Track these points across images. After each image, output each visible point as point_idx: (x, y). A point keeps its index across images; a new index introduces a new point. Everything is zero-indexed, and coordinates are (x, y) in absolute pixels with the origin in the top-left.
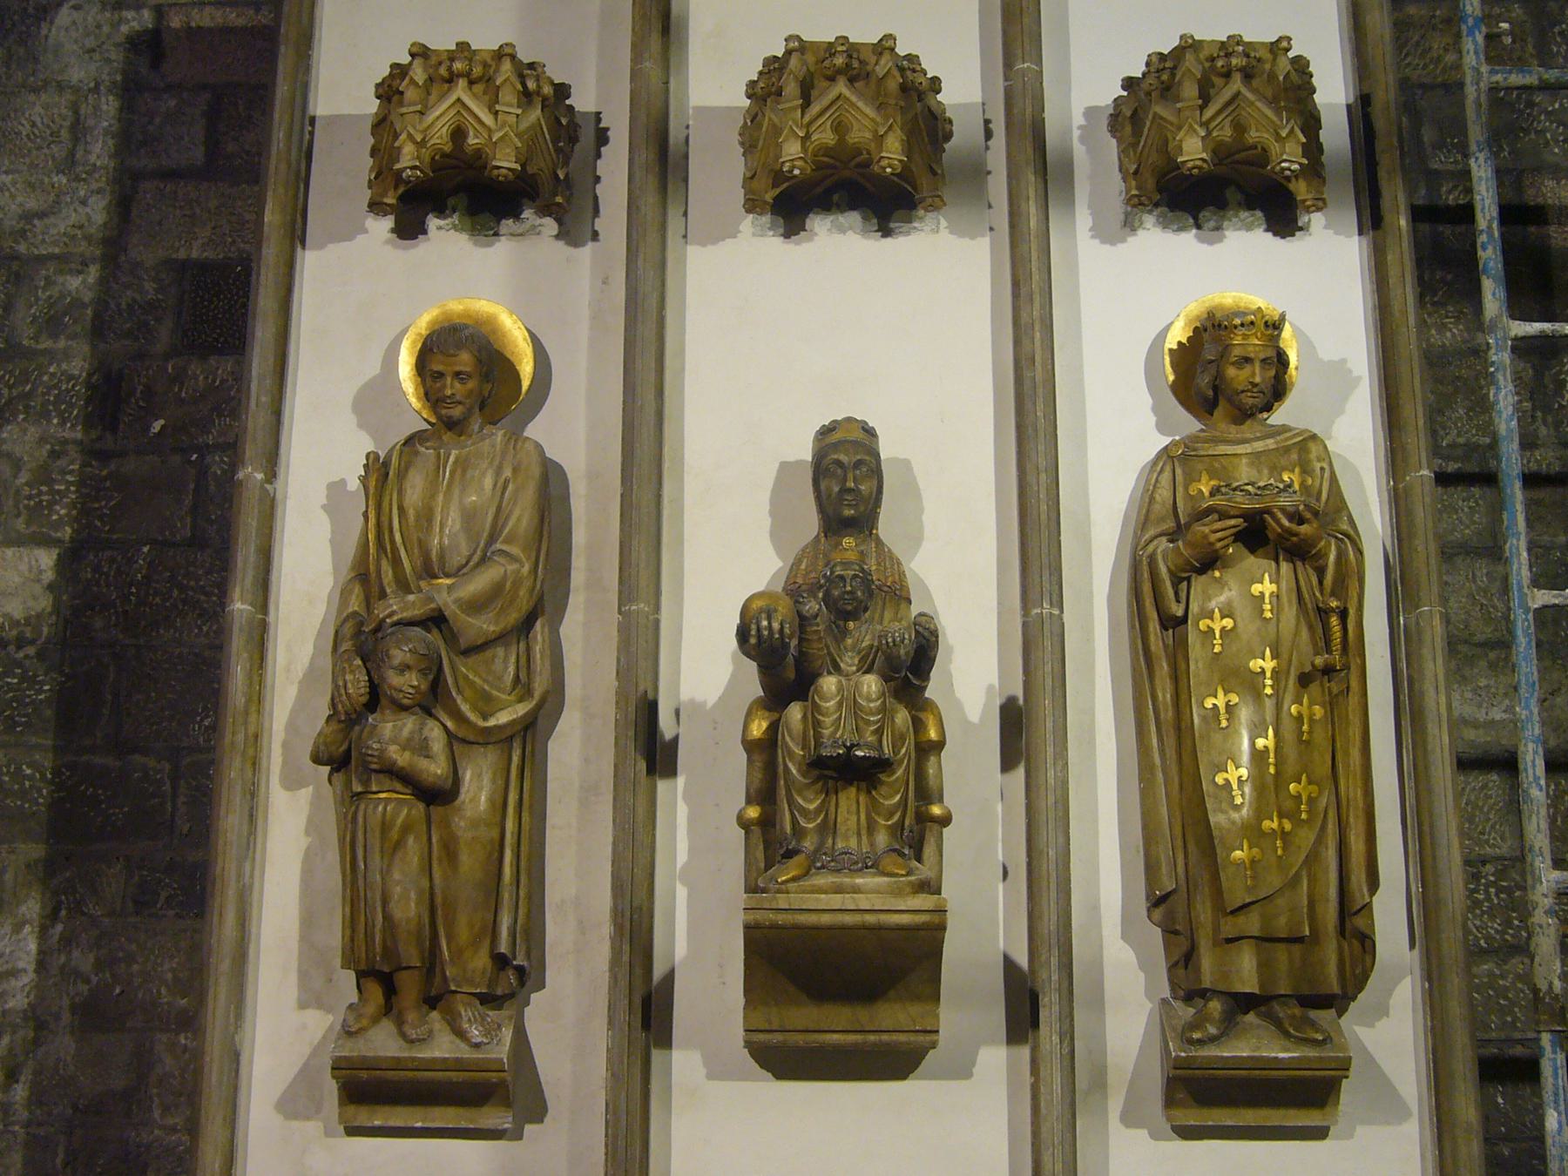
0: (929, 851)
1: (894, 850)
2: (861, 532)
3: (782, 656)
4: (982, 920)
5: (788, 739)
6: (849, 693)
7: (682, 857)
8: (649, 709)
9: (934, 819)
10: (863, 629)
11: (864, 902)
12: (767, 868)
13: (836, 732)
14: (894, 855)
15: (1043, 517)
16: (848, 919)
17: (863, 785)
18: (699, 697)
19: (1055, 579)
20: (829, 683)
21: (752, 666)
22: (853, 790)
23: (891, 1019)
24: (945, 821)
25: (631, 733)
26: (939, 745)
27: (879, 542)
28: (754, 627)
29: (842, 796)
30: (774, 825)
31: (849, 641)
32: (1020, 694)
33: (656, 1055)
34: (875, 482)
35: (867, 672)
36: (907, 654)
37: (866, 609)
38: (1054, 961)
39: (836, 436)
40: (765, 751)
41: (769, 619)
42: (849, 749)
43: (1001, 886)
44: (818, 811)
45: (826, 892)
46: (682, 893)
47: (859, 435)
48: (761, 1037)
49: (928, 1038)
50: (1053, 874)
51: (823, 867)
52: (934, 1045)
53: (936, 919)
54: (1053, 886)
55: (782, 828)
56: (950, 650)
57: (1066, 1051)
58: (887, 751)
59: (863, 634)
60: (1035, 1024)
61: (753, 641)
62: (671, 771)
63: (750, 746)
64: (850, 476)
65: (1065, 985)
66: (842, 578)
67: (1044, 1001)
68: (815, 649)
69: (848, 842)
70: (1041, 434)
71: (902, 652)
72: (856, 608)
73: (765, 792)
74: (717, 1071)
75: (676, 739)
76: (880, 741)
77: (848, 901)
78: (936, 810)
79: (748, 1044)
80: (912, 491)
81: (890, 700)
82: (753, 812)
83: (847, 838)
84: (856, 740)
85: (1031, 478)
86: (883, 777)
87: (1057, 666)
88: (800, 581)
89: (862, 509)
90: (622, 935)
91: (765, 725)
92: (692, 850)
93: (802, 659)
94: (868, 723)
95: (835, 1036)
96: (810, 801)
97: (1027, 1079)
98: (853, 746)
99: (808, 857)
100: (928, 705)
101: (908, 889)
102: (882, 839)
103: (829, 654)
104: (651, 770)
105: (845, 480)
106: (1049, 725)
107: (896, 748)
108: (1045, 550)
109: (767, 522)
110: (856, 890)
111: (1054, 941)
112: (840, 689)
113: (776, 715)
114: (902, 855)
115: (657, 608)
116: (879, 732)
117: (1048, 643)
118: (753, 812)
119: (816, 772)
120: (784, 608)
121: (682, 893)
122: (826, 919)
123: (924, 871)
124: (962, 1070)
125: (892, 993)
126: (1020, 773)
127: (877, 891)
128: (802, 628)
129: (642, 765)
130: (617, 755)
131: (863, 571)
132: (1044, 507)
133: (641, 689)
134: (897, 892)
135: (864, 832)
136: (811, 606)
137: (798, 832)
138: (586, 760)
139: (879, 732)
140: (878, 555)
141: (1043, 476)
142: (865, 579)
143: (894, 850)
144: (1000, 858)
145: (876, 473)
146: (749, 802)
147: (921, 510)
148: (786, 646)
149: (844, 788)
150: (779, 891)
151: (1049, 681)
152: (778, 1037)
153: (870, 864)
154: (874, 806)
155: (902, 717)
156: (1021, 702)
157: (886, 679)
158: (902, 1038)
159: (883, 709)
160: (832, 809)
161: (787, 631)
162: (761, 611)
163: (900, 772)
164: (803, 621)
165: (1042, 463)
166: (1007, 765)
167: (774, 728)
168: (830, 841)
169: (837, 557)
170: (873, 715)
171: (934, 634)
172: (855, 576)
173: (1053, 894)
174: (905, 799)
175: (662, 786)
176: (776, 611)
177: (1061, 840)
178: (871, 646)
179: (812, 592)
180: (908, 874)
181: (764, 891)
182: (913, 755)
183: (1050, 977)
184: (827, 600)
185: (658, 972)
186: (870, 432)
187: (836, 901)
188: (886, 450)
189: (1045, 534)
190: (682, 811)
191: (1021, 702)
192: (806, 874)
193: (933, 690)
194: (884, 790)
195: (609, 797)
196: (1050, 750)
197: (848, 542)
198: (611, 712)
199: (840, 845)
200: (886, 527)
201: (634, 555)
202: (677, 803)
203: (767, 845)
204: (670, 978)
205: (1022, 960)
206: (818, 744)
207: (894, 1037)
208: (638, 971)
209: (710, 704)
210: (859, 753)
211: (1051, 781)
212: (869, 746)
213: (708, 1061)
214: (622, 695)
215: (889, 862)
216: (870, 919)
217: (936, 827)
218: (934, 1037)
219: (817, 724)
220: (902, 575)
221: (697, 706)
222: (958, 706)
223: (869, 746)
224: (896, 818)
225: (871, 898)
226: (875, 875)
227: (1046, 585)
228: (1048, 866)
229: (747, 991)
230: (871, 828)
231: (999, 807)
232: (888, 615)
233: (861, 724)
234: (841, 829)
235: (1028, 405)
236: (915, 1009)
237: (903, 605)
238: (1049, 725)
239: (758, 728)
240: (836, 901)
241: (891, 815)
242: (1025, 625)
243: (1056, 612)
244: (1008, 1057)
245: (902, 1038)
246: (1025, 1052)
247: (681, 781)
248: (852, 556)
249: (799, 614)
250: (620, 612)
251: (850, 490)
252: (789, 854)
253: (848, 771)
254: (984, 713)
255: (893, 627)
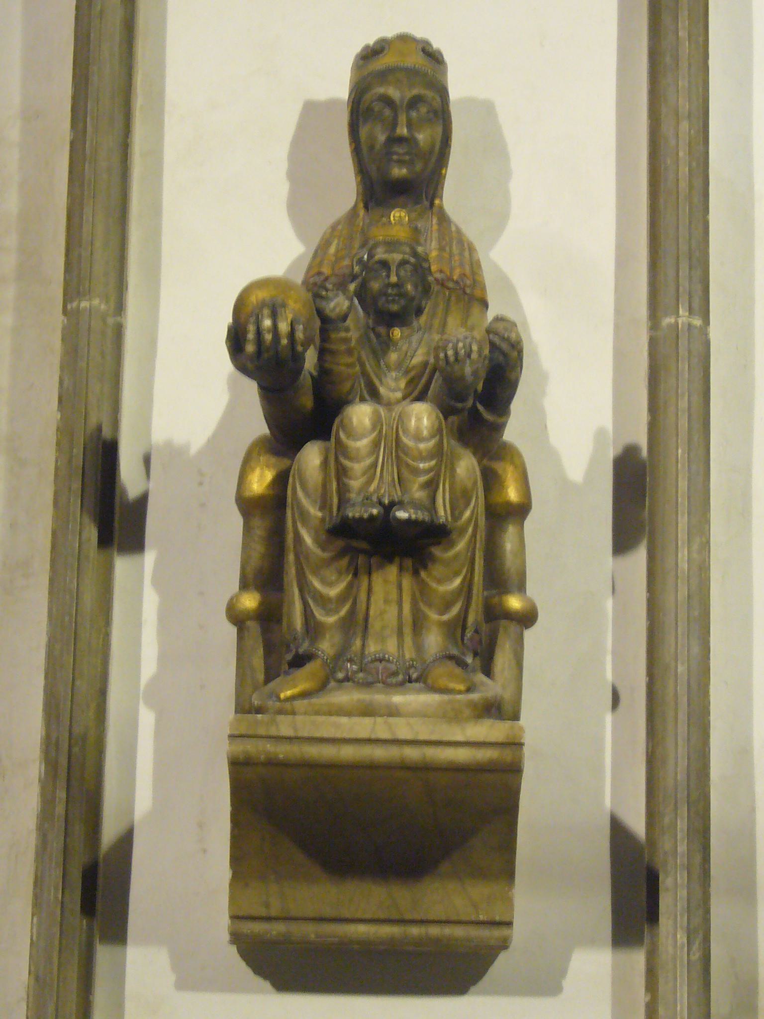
0: (502, 660)
1: (451, 658)
2: (417, 202)
3: (294, 374)
4: (577, 765)
5: (300, 494)
6: (389, 430)
7: (149, 667)
8: (106, 454)
9: (510, 616)
10: (415, 338)
11: (403, 729)
12: (268, 679)
13: (369, 486)
14: (451, 666)
15: (683, 185)
16: (380, 753)
17: (409, 563)
18: (179, 437)
19: (697, 273)
20: (361, 414)
21: (251, 388)
22: (392, 571)
23: (443, 903)
24: (528, 618)
25: (77, 485)
26: (522, 510)
27: (443, 219)
28: (252, 328)
29: (378, 579)
30: (279, 621)
31: (393, 357)
32: (643, 441)
33: (103, 954)
34: (439, 130)
35: (420, 398)
36: (475, 373)
37: (419, 311)
38: (682, 825)
39: (386, 60)
40: (268, 513)
41: (274, 316)
42: (388, 508)
43: (609, 718)
44: (342, 599)
45: (349, 714)
46: (147, 719)
47: (416, 60)
48: (257, 928)
49: (497, 933)
50: (683, 700)
51: (347, 679)
52: (504, 945)
53: (507, 755)
54: (682, 717)
55: (290, 625)
56: (543, 378)
57: (696, 956)
58: (443, 513)
59: (413, 347)
60: (653, 916)
61: (250, 348)
62: (135, 543)
63: (248, 506)
64: (402, 118)
65: (698, 859)
66: (385, 264)
67: (666, 882)
68: (343, 366)
69: (385, 644)
70: (684, 64)
71: (468, 370)
72: (405, 309)
73: (268, 573)
74: (189, 979)
75: (143, 500)
76: (433, 500)
77: (379, 728)
78: (514, 603)
79: (236, 938)
80: (495, 147)
81: (450, 443)
82: (250, 602)
83: (382, 639)
84: (397, 494)
85: (667, 128)
86: (436, 551)
87: (697, 400)
88: (326, 270)
89: (418, 167)
90: (55, 777)
91: (269, 476)
92: (163, 658)
93: (324, 376)
94: (416, 472)
95: (362, 930)
96: (331, 584)
97: (641, 996)
98: (392, 504)
99: (325, 663)
100: (507, 453)
101: (467, 712)
102: (434, 641)
103: (364, 374)
104: (106, 540)
105: (394, 124)
106: (683, 485)
107: (455, 510)
108: (683, 232)
109: (283, 188)
110: (393, 712)
111: (682, 795)
112: (377, 422)
113: (286, 462)
114: (461, 663)
115: (120, 307)
116: (431, 486)
117: (684, 366)
118: (250, 602)
119: (340, 543)
120: (296, 306)
121: (147, 719)
122: (348, 753)
123: (492, 688)
124: (546, 983)
125: (445, 867)
126: (639, 557)
127: (422, 714)
128: (324, 333)
129: (92, 533)
130: (56, 518)
131: (415, 254)
132: (684, 170)
133: (93, 421)
134: (454, 716)
135: (408, 630)
136: (338, 304)
137: (313, 629)
138: (13, 526)
139: (431, 486)
140: (441, 239)
141: (684, 126)
142: (419, 267)
143: (451, 658)
144: (609, 675)
145: (441, 115)
146: (244, 585)
147: (506, 174)
148: (297, 358)
149: (381, 567)
150: (281, 712)
151: (683, 423)
152: (277, 929)
153: (415, 676)
154: (422, 592)
155: (466, 465)
156: (644, 453)
157: (447, 411)
158: (458, 932)
159: (438, 453)
160: (363, 596)
161: (300, 335)
162: (263, 304)
163: (461, 545)
164: (327, 324)
165: (684, 106)
166: (622, 544)
167: (282, 480)
168: (358, 643)
169: (379, 234)
170: (423, 459)
171: (517, 347)
172: (403, 263)
173: (682, 729)
174: (468, 585)
175: (122, 565)
176: (284, 305)
177: (696, 650)
178: (425, 364)
179: (342, 286)
180: (469, 690)
181: (259, 710)
182: (482, 522)
183: (675, 849)
184: (362, 294)
185: (109, 832)
186: (435, 58)
187: (363, 727)
188: (459, 86)
189: (684, 209)
190: (151, 601)
191: (644, 453)
192: (322, 687)
193: (514, 432)
194: (437, 570)
195: (44, 579)
196: (683, 522)
197: (397, 214)
198: (49, 456)
199: (373, 648)
200: (455, 195)
201: (87, 228)
202: (142, 587)
203: (269, 649)
204: (126, 841)
205: (637, 824)
206: (343, 501)
207: (448, 931)
208: (78, 829)
209: (194, 450)
210: (402, 515)
211: (683, 565)
212: (416, 505)
213: (178, 963)
214: (65, 431)
215: (443, 674)
216: (412, 754)
217: (513, 627)
218: (504, 931)
219: (342, 473)
220: (475, 266)
221: (175, 452)
222: (553, 456)
223: (416, 505)
224: (455, 610)
225: (413, 725)
226: (419, 691)
227: (684, 283)
228: (677, 689)
229: (237, 858)
230: (418, 625)
231: (609, 604)
232: (453, 322)
233: (406, 474)
234: (375, 625)
235: (666, 18)
236: (479, 890)
237: (476, 310)
238: (683, 485)
239: (260, 481)
240: (363, 727)
241: (448, 606)
242: (653, 343)
243: (697, 322)
244: (615, 967)
245: (458, 932)
246: (638, 958)
247: (150, 557)
248: (401, 233)
249: (320, 313)
250: (65, 312)
251: (401, 140)
252: (299, 661)
253: (387, 541)
254: (594, 462)
255: (461, 335)
